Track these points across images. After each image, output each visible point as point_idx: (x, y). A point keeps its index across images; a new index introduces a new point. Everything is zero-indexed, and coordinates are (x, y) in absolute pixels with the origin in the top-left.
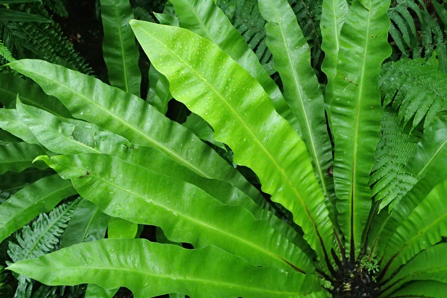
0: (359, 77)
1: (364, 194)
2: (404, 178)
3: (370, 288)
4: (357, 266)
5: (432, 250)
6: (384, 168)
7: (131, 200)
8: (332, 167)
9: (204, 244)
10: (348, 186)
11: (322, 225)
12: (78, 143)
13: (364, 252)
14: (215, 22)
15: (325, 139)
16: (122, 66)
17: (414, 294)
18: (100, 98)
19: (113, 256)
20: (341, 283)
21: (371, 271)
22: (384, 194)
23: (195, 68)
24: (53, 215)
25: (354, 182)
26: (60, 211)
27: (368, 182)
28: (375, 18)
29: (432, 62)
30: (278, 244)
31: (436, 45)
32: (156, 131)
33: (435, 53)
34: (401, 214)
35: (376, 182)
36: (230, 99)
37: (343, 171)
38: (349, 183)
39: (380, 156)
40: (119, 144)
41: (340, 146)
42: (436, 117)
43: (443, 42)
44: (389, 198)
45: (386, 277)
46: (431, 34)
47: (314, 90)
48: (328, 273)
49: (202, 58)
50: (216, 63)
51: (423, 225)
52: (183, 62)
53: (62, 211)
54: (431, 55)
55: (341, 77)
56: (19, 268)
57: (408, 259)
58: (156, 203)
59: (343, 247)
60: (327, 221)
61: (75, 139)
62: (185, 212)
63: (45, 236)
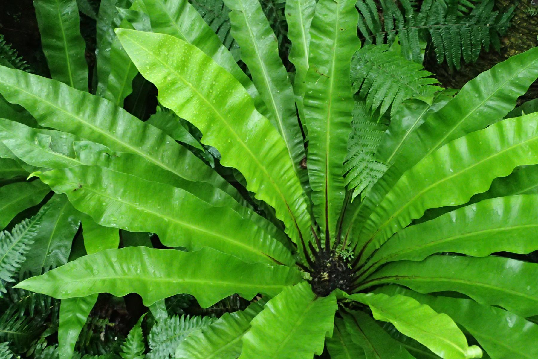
0: (330, 69)
1: (338, 184)
2: (376, 166)
3: (346, 275)
4: (332, 255)
5: (403, 232)
6: (355, 157)
7: (123, 209)
8: (306, 159)
9: (197, 247)
10: (322, 177)
11: (301, 218)
12: (57, 154)
13: (339, 241)
14: (186, 17)
15: (296, 132)
16: (65, 60)
17: (388, 276)
18: (67, 103)
19: (117, 266)
20: (319, 273)
21: (347, 259)
22: (355, 183)
23: (180, 73)
24: (16, 231)
25: (328, 173)
26: (24, 227)
27: (341, 173)
28: (344, 11)
29: (394, 48)
30: (261, 240)
31: (398, 30)
32: (129, 134)
33: (397, 39)
34: (373, 201)
35: (348, 172)
36: (214, 101)
37: (317, 163)
38: (322, 174)
39: (350, 146)
40: (100, 153)
41: (314, 138)
42: (402, 105)
43: (404, 27)
44: (362, 186)
45: (361, 263)
46: (392, 19)
47: (284, 81)
48: (306, 264)
49: (187, 63)
50: (200, 67)
51: (395, 210)
52: (168, 68)
53: (26, 227)
54: (393, 40)
55: (313, 70)
56: (28, 286)
57: (382, 243)
58: (151, 211)
59: (319, 238)
60: (306, 214)
61: (53, 151)
62: (174, 215)
63: (9, 255)
